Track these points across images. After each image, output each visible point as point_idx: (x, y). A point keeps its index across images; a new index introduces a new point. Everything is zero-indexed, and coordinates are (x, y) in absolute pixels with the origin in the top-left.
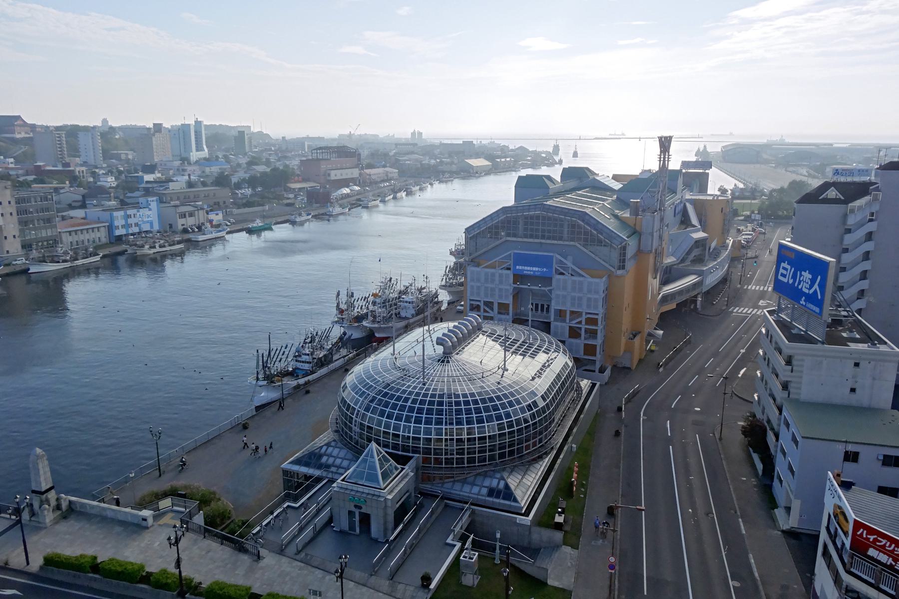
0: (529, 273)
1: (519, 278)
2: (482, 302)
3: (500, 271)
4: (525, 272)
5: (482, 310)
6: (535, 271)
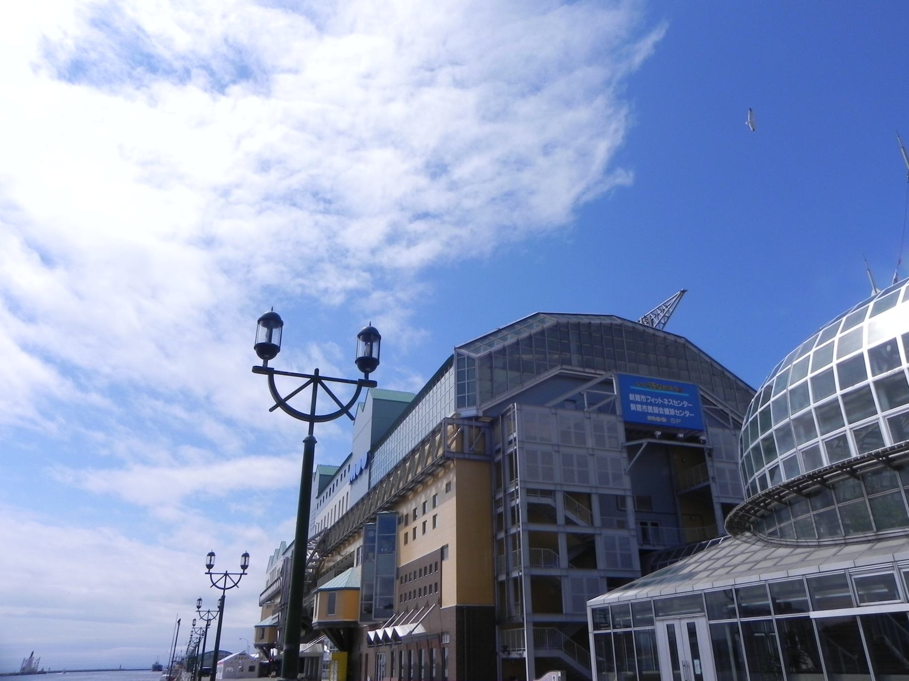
0: (658, 419)
2: (560, 498)
4: (650, 418)
5: (561, 519)
6: (668, 417)
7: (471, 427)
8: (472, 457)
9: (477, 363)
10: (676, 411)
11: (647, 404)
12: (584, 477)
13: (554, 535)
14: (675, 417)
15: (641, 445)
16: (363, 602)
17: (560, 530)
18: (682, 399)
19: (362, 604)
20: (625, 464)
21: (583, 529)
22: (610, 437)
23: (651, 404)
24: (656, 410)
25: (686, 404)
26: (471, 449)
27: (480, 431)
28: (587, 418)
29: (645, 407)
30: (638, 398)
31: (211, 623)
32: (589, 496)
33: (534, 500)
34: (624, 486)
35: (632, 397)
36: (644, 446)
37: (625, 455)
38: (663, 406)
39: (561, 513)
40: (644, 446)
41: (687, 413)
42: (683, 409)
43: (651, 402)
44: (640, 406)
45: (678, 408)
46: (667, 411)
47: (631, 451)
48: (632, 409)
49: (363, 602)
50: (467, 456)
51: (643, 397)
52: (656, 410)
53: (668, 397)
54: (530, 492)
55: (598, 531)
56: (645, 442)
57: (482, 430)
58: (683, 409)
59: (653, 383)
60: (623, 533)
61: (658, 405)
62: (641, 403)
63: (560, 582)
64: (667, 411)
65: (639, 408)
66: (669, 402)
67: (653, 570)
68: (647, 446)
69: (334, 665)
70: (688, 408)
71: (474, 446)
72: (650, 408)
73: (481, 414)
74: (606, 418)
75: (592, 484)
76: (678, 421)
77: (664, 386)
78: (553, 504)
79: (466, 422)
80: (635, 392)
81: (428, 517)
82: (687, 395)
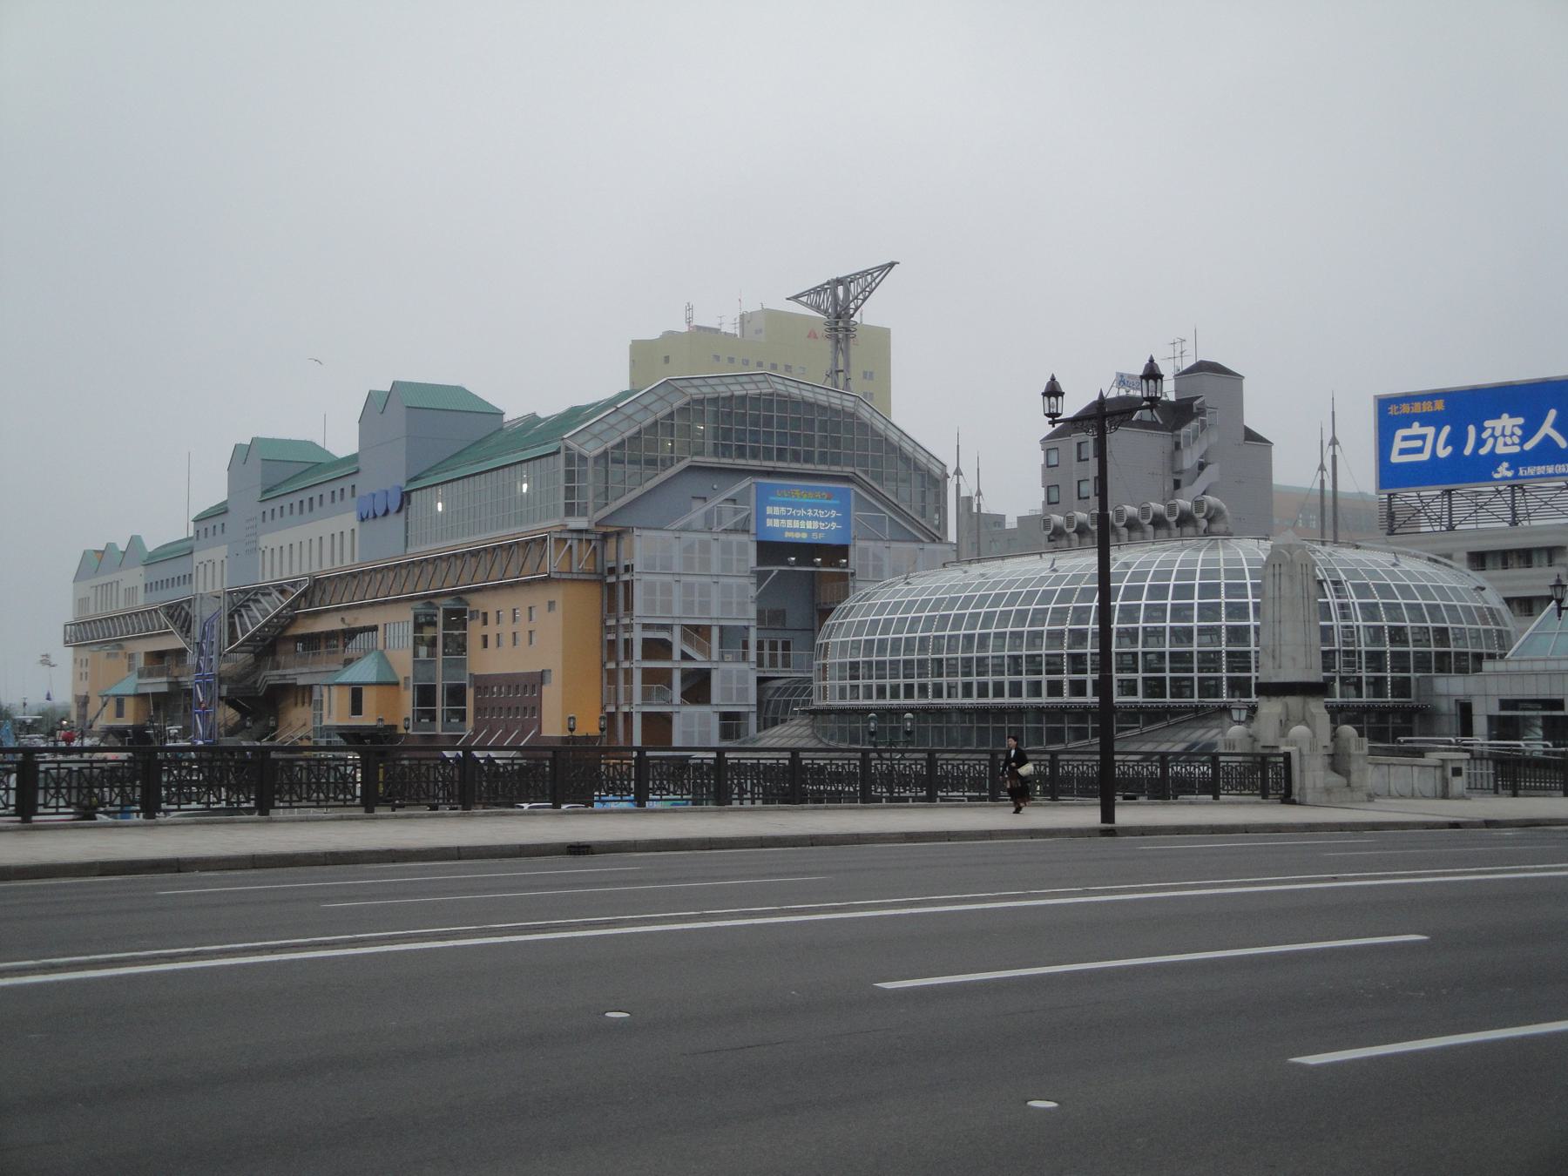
0: (797, 535)
1: (771, 551)
2: (677, 631)
3: (723, 537)
4: (787, 535)
5: (676, 655)
6: (809, 532)
7: (580, 540)
8: (581, 577)
9: (591, 462)
10: (821, 524)
11: (786, 517)
12: (705, 606)
13: (669, 671)
14: (819, 531)
15: (772, 571)
16: (445, 707)
17: (676, 665)
18: (829, 507)
19: (443, 710)
20: (753, 592)
21: (700, 663)
22: (738, 560)
23: (792, 517)
24: (796, 524)
25: (834, 513)
26: (580, 567)
27: (591, 544)
28: (715, 539)
29: (783, 521)
30: (777, 510)
31: (71, 585)
32: (709, 628)
33: (650, 635)
34: (747, 616)
35: (769, 510)
36: (774, 574)
37: (754, 580)
38: (806, 518)
39: (678, 646)
40: (774, 574)
41: (834, 525)
42: (829, 520)
43: (792, 514)
44: (778, 520)
45: (823, 520)
46: (809, 525)
47: (761, 577)
48: (768, 525)
49: (445, 707)
50: (575, 576)
51: (783, 509)
52: (796, 524)
53: (813, 506)
54: (646, 627)
55: (715, 666)
56: (776, 569)
57: (593, 543)
58: (829, 520)
59: (797, 490)
60: (744, 666)
61: (800, 518)
62: (780, 517)
63: (671, 717)
64: (809, 525)
65: (776, 523)
66: (814, 513)
67: (775, 723)
68: (778, 574)
69: (296, 697)
70: (836, 519)
71: (583, 562)
72: (789, 522)
73: (592, 526)
74: (736, 538)
75: (715, 614)
76: (821, 536)
77: (810, 494)
78: (670, 639)
79: (575, 535)
80: (773, 504)
81: (522, 627)
82: (837, 502)
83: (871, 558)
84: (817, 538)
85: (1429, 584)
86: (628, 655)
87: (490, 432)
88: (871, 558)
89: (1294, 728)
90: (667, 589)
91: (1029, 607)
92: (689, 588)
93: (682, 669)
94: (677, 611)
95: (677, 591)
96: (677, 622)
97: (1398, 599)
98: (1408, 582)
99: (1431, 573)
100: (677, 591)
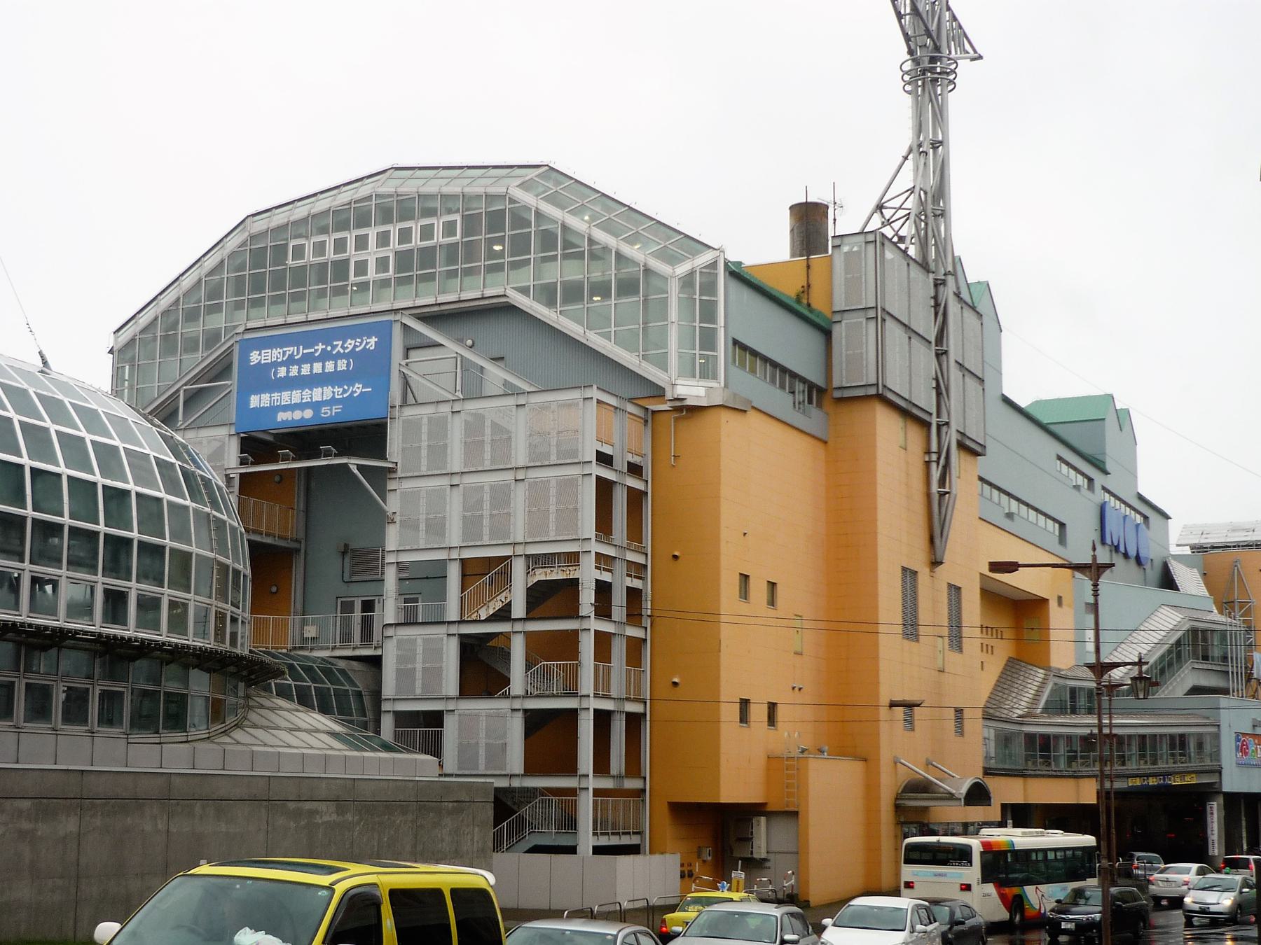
0: (297, 415)
4: (282, 416)
6: (316, 406)
10: (336, 390)
14: (333, 402)
76: (336, 409)
83: (488, 431)
84: (330, 414)
85: (89, 437)
86: (603, 589)
87: (912, 300)
88: (488, 431)
89: (100, 925)
90: (501, 497)
91: (167, 536)
92: (539, 489)
93: (461, 636)
94: (454, 537)
95: (519, 496)
96: (520, 550)
97: (94, 474)
98: (83, 433)
99: (58, 395)
100: (519, 496)
